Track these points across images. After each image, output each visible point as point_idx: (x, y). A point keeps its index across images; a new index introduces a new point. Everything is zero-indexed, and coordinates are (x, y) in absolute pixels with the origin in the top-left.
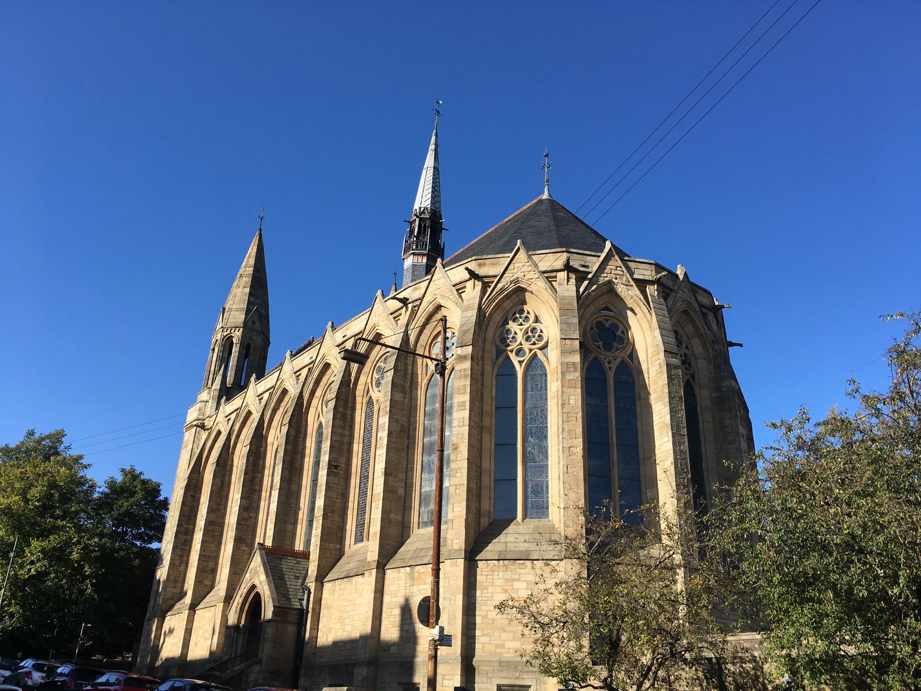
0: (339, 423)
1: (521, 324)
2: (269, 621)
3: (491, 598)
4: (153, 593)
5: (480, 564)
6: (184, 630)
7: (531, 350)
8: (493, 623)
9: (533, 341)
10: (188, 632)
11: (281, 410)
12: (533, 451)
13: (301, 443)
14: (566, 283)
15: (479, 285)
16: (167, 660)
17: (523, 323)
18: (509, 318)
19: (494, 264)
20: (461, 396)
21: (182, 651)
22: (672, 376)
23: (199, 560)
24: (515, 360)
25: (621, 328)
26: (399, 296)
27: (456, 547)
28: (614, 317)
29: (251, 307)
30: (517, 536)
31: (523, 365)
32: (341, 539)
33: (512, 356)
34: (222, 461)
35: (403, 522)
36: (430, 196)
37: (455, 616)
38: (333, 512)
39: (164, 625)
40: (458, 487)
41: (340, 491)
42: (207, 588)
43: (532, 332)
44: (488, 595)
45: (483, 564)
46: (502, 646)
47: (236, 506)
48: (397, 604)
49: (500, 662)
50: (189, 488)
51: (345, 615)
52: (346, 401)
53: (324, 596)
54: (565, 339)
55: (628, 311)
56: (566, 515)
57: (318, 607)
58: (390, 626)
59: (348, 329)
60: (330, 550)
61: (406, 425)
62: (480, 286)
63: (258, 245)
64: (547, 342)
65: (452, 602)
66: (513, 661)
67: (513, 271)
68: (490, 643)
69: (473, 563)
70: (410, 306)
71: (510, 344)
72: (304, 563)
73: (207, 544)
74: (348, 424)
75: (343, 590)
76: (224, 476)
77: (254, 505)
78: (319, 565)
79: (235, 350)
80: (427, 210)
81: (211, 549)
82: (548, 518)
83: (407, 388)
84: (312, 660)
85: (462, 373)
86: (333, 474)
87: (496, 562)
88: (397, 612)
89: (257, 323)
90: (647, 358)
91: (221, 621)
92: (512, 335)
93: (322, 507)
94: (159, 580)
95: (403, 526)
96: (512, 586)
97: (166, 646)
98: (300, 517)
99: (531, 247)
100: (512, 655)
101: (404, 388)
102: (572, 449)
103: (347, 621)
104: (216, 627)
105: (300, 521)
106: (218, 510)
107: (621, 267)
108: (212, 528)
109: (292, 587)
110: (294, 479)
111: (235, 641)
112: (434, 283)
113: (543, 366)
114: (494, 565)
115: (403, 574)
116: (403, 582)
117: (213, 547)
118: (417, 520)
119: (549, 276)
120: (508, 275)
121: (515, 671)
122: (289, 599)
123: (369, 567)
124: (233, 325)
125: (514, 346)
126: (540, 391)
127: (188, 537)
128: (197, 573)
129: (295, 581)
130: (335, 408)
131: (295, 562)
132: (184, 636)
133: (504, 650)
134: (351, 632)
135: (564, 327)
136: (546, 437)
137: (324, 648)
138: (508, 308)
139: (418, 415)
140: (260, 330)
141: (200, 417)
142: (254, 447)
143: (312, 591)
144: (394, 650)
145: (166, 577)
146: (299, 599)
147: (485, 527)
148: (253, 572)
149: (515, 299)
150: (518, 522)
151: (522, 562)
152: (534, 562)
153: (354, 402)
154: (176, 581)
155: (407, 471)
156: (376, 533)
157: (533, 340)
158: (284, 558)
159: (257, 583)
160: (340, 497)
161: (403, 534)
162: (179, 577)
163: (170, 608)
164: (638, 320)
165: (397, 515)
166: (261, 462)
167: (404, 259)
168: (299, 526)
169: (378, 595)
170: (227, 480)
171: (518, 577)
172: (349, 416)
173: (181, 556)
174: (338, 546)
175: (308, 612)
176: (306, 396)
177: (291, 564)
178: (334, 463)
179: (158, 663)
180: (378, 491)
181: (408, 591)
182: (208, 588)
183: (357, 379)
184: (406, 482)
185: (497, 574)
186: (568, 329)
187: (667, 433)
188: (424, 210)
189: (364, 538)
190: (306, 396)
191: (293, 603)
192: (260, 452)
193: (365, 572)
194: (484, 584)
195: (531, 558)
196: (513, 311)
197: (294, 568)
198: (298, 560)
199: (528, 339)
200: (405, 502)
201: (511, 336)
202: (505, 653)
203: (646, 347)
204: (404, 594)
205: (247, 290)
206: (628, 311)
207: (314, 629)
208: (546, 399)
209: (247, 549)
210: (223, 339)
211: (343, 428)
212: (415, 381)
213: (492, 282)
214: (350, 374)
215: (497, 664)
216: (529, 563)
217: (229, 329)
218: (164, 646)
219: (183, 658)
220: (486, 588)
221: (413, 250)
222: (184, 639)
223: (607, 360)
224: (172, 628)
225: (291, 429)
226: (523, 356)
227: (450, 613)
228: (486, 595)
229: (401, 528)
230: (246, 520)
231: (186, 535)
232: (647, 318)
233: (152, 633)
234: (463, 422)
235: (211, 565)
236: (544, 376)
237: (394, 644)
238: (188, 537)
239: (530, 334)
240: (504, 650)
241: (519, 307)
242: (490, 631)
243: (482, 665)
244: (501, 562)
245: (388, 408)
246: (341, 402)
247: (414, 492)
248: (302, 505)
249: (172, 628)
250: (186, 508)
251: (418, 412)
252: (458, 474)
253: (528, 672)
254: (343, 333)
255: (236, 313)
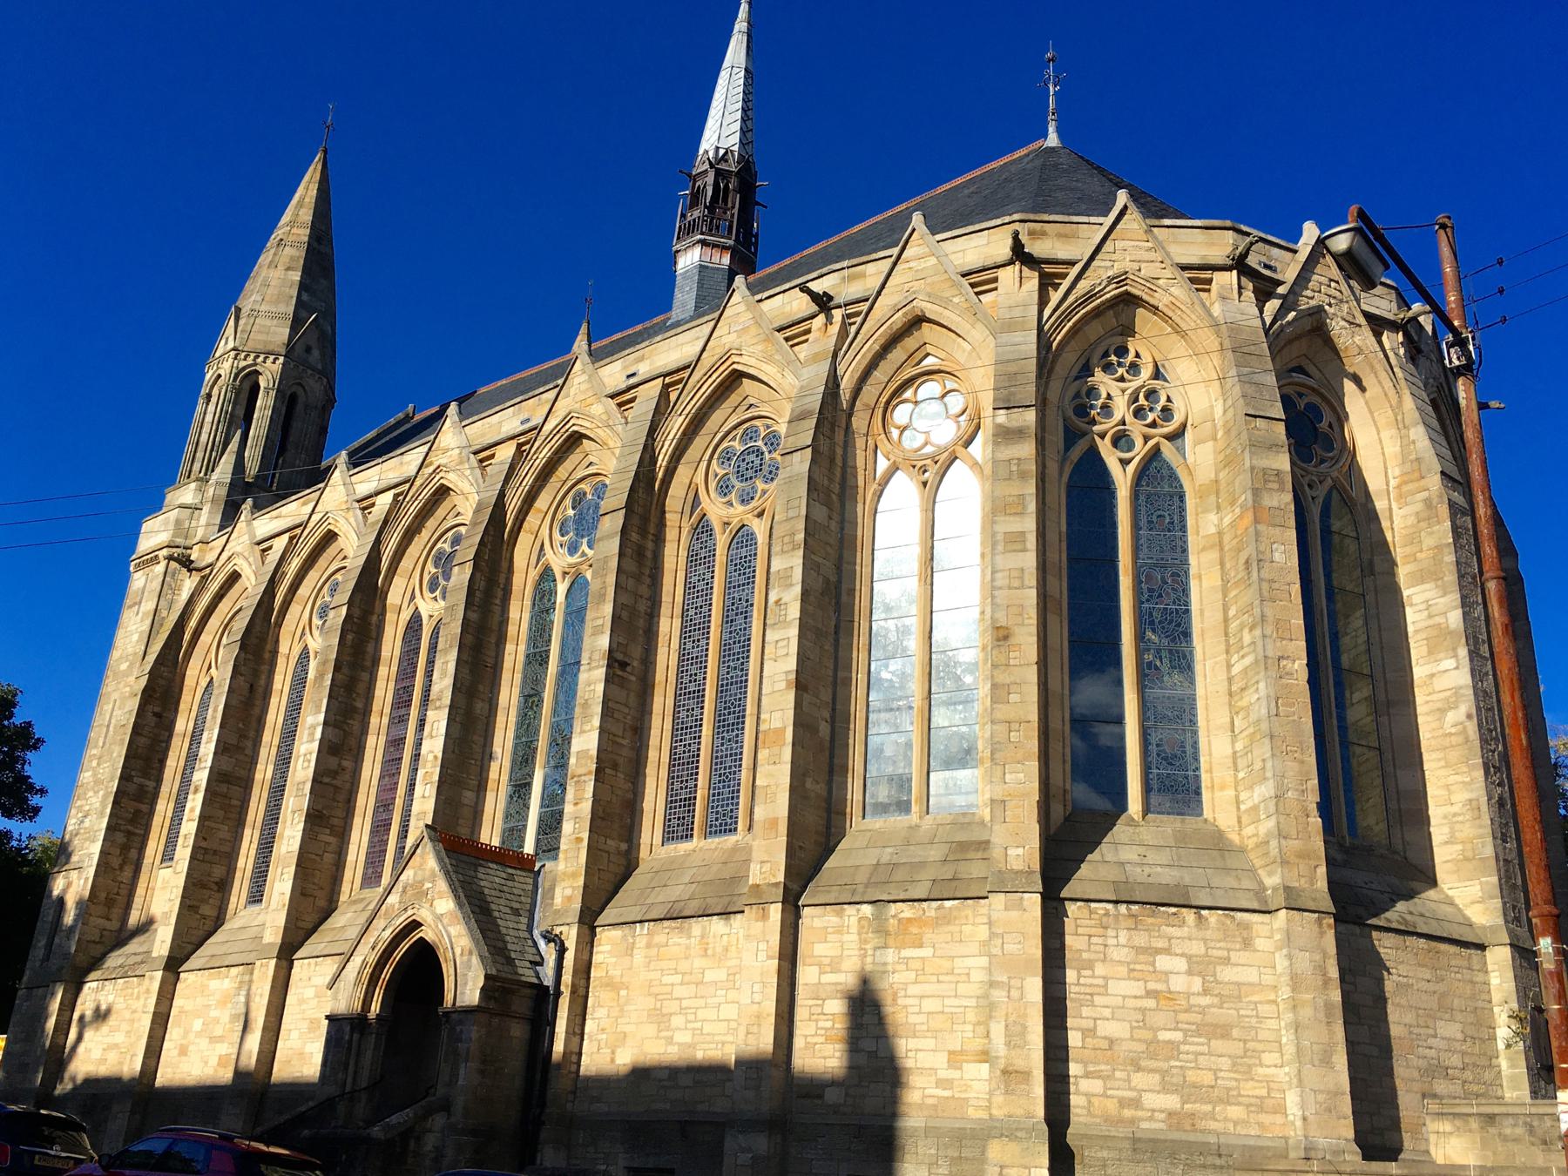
0: (631, 566)
1: (1122, 379)
2: (469, 1011)
3: (669, 997)
4: (43, 926)
5: (1072, 908)
6: (150, 1016)
7: (1146, 439)
8: (1110, 1049)
9: (1149, 420)
10: (161, 1021)
11: (425, 534)
12: (1158, 664)
13: (497, 609)
14: (1236, 296)
15: (1032, 282)
16: (92, 1083)
17: (1126, 375)
18: (1095, 360)
19: (1066, 236)
20: (1012, 518)
21: (144, 1062)
22: (1457, 528)
23: (193, 858)
24: (1111, 457)
25: (1328, 417)
26: (814, 286)
27: (1017, 865)
28: (1313, 390)
29: (304, 314)
30: (1141, 850)
31: (1131, 468)
32: (631, 832)
33: (1105, 448)
34: (253, 640)
35: (828, 800)
36: (737, 126)
37: (1025, 1027)
38: (615, 766)
39: (80, 1001)
40: (1015, 726)
41: (629, 720)
42: (207, 922)
43: (1147, 397)
44: (1096, 981)
45: (1079, 908)
46: (1136, 1103)
47: (312, 741)
48: (839, 988)
49: (1135, 1140)
50: (150, 696)
51: (672, 1006)
52: (645, 519)
53: (596, 958)
54: (1255, 417)
55: (1345, 380)
56: (1281, 809)
57: (583, 982)
58: (822, 1039)
59: (642, 359)
60: (608, 852)
61: (833, 579)
62: (1036, 281)
63: (320, 183)
64: (1184, 426)
65: (1015, 993)
66: (1166, 1141)
67: (1114, 257)
68: (1105, 1095)
69: (1055, 904)
70: (837, 314)
71: (1097, 418)
72: (522, 880)
73: (213, 825)
74: (647, 572)
75: (659, 946)
76: (256, 673)
77: (353, 742)
78: (586, 886)
79: (264, 405)
80: (733, 155)
81: (221, 835)
82: (1201, 814)
83: (834, 497)
84: (569, 1105)
85: (1014, 468)
86: (616, 679)
87: (1110, 906)
88: (837, 1007)
89: (316, 353)
90: (1388, 485)
91: (270, 1002)
92: (1101, 401)
93: (594, 753)
94: (61, 901)
95: (829, 811)
96: (1153, 964)
97: (88, 1051)
98: (493, 775)
99: (1155, 207)
100: (1162, 1126)
101: (829, 496)
102: (1284, 662)
103: (677, 1021)
104: (253, 1015)
105: (491, 785)
106: (239, 749)
107: (1337, 282)
108: (223, 788)
109: (512, 932)
110: (481, 688)
111: (353, 1051)
112: (907, 265)
113: (1173, 477)
114: (1107, 914)
115: (854, 920)
116: (855, 937)
117: (224, 832)
118: (861, 798)
119: (1198, 275)
120: (1103, 264)
121: (1172, 1163)
122: (510, 962)
123: (761, 898)
124: (260, 347)
125: (1107, 425)
126: (1169, 531)
127: (144, 808)
128: (185, 888)
129: (513, 917)
130: (624, 531)
131: (504, 875)
132: (151, 1029)
133: (1140, 1113)
134: (692, 1046)
135: (1251, 390)
136: (1187, 634)
137: (604, 1084)
138: (1093, 338)
139: (859, 561)
140: (320, 367)
141: (179, 541)
142: (357, 612)
143: (571, 944)
144: (831, 1096)
145: (87, 893)
146: (531, 962)
147: (1059, 824)
148: (410, 892)
149: (1110, 319)
150: (1133, 819)
151: (1173, 910)
152: (1203, 912)
153: (662, 524)
154: (109, 903)
155: (835, 684)
156: (774, 822)
157: (1151, 417)
158: (481, 865)
159: (423, 914)
160: (629, 734)
161: (828, 827)
162: (118, 894)
163: (96, 963)
164: (1367, 403)
165: (818, 783)
166: (370, 648)
167: (677, 252)
168: (490, 797)
169: (786, 965)
170: (262, 682)
171: (1166, 945)
172: (649, 554)
173: (125, 848)
174: (624, 846)
175: (558, 993)
176: (513, 505)
177: (497, 880)
178: (619, 656)
179: (59, 1090)
180: (776, 724)
181: (869, 960)
182: (209, 924)
183: (670, 472)
184: (834, 710)
185: (1114, 934)
186: (1257, 395)
187: (1454, 649)
188: (726, 153)
189: (695, 832)
190: (513, 505)
191: (521, 971)
192: (370, 624)
193: (747, 909)
194: (1085, 956)
195: (1194, 903)
196: (1100, 351)
197: (505, 888)
198: (510, 871)
199: (1139, 413)
200: (832, 756)
201: (1099, 403)
202: (1143, 1120)
203: (1385, 463)
204: (858, 967)
205: (296, 276)
206: (1345, 380)
207: (574, 1033)
208: (1185, 550)
209: (331, 839)
210: (237, 375)
211: (638, 578)
212: (850, 482)
213: (1064, 276)
214: (654, 460)
215: (1126, 1144)
216: (1189, 915)
217: (252, 355)
218: (81, 1049)
219: (145, 1081)
220: (1090, 965)
221: (702, 233)
222: (150, 1037)
223: (1307, 479)
224: (103, 1007)
225: (478, 575)
226: (1129, 450)
227: (1011, 1019)
228: (1089, 981)
229: (825, 815)
230: (334, 774)
231: (141, 802)
232: (1389, 401)
233: (46, 1018)
234: (1022, 578)
235: (218, 872)
236: (1176, 499)
237: (834, 1083)
238: (144, 808)
239: (1142, 401)
240: (1140, 1113)
241: (1118, 340)
242: (1103, 1067)
243: (1091, 1147)
244: (1123, 908)
245: (801, 536)
246: (636, 520)
247: (851, 733)
248: (497, 749)
249: (103, 1007)
250: (142, 741)
251: (859, 554)
252: (1013, 698)
253: (1204, 1166)
254: (625, 368)
255: (268, 322)
